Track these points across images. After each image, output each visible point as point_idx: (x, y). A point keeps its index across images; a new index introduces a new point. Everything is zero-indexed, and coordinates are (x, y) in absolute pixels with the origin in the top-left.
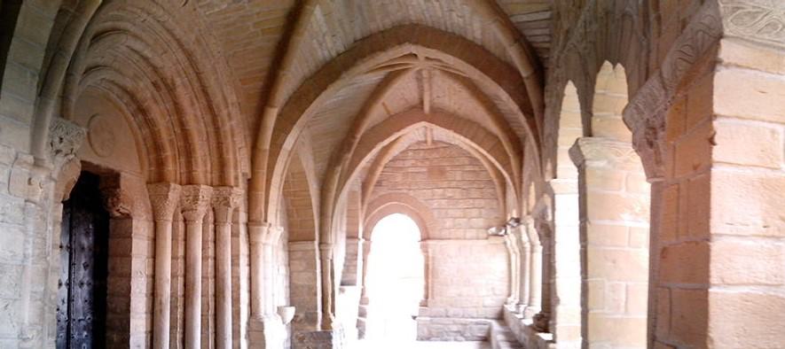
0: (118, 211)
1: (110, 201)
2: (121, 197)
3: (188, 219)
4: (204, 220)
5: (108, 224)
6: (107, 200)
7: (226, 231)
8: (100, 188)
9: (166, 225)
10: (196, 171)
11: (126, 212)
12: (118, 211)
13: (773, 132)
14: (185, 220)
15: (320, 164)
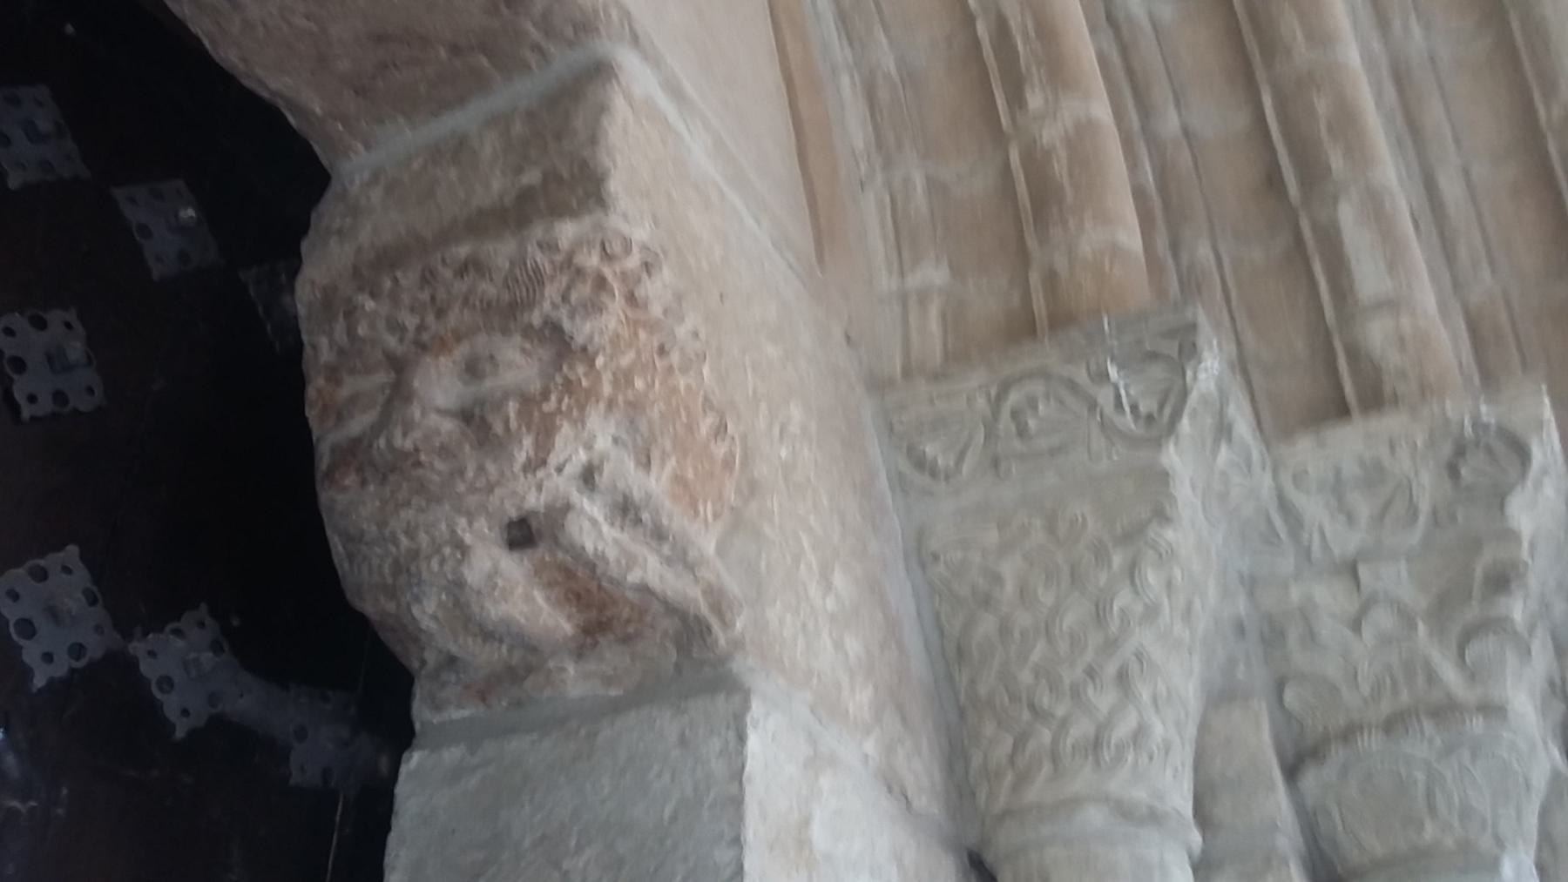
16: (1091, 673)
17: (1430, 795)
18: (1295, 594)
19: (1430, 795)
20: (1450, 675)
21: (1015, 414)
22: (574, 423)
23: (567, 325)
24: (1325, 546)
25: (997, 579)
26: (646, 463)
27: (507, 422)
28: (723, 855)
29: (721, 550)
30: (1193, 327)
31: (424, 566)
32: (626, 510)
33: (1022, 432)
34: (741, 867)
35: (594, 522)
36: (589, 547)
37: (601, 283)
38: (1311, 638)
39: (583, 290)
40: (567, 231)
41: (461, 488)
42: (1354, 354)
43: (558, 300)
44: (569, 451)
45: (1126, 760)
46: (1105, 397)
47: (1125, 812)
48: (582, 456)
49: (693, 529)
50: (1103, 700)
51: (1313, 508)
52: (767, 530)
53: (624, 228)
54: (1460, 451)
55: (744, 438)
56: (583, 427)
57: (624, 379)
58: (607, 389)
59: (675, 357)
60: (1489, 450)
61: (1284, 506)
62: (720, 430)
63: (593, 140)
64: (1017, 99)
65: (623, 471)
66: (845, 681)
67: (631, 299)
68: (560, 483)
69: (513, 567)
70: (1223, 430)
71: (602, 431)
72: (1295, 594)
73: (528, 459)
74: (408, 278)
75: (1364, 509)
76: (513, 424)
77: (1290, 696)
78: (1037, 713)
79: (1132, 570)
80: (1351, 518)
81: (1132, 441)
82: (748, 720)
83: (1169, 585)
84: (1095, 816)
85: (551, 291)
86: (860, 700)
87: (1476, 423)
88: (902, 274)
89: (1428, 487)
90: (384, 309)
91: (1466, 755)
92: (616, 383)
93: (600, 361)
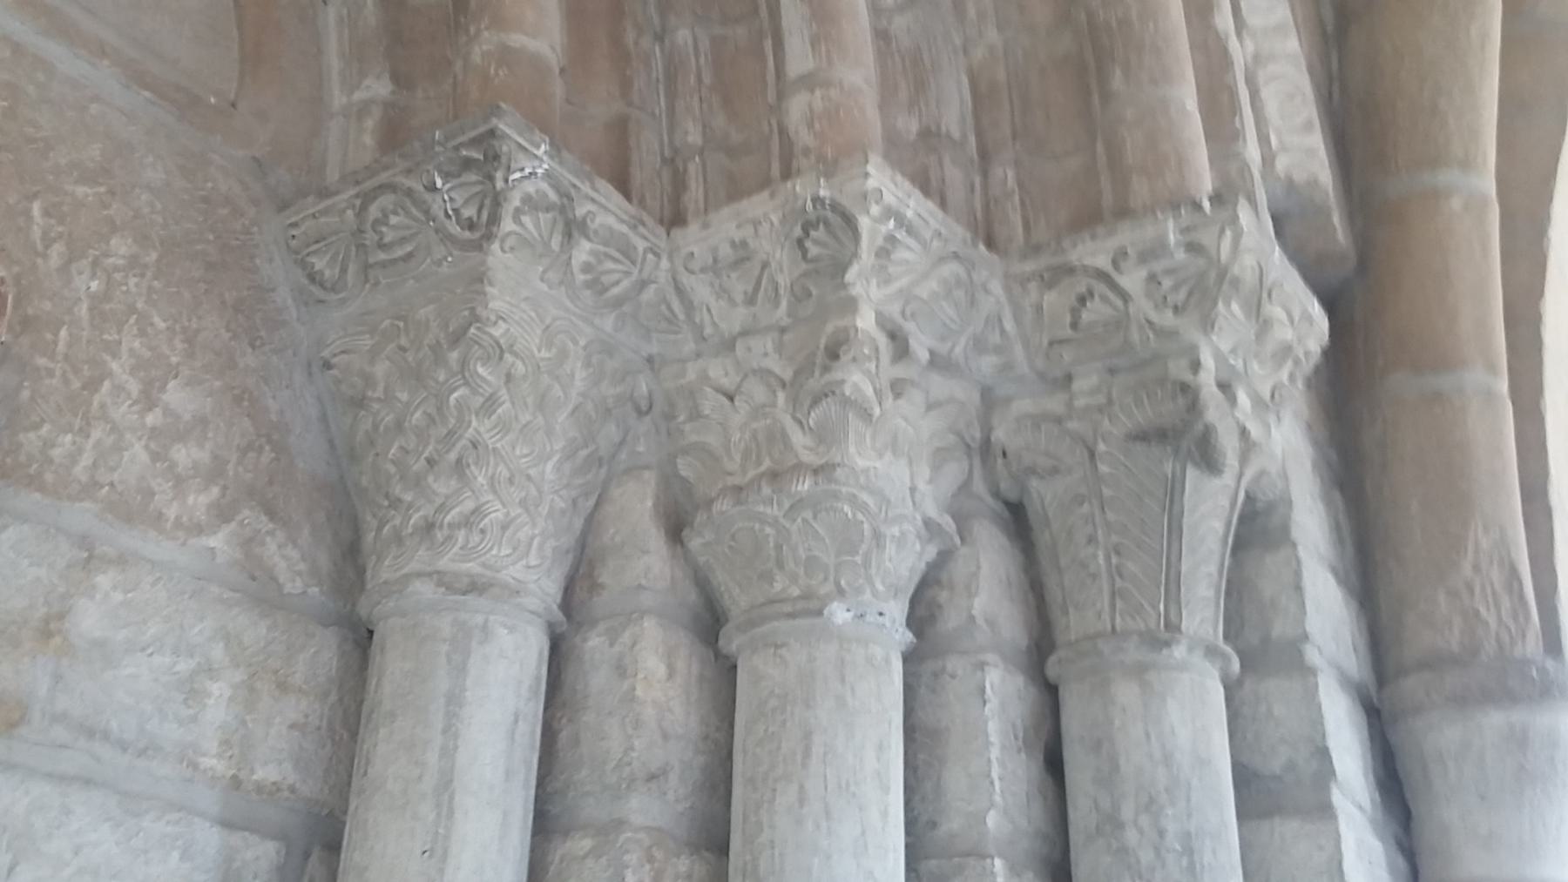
17: (779, 547)
18: (692, 373)
19: (779, 547)
20: (798, 439)
25: (369, 381)
38: (696, 415)
45: (457, 540)
46: (437, 209)
47: (445, 581)
50: (441, 486)
51: (701, 289)
54: (807, 227)
60: (827, 224)
72: (692, 373)
78: (395, 503)
81: (467, 246)
87: (817, 200)
89: (784, 266)
91: (808, 514)
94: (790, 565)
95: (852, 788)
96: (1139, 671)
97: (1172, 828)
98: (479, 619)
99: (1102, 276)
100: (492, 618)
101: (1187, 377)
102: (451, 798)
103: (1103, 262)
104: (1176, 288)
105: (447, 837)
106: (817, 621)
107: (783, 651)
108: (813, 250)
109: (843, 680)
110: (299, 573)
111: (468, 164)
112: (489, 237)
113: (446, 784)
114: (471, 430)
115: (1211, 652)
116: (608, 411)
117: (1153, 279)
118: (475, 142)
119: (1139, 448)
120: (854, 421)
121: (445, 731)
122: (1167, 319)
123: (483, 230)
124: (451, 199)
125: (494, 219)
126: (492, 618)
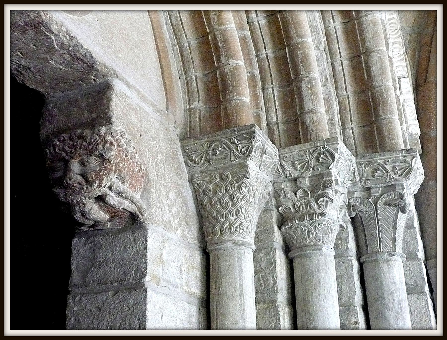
0: (101, 199)
1: (75, 167)
2: (113, 154)
3: (294, 241)
4: (336, 247)
5: (68, 253)
6: (66, 163)
7: (387, 280)
8: (43, 133)
9: (240, 257)
10: (312, 112)
11: (127, 205)
12: (101, 199)
13: (393, 44)
14: (287, 249)
15: (225, 17)
16: (230, 212)
21: (213, 150)
22: (107, 177)
23: (104, 155)
24: (290, 174)
26: (123, 183)
27: (92, 177)
28: (143, 266)
29: (142, 197)
30: (254, 132)
31: (76, 207)
32: (119, 194)
33: (215, 154)
34: (146, 268)
35: (112, 197)
36: (112, 203)
37: (111, 144)
39: (108, 145)
40: (103, 130)
41: (83, 192)
42: (303, 123)
43: (102, 148)
44: (106, 182)
47: (235, 243)
48: (109, 183)
49: (134, 194)
51: (287, 166)
52: (152, 190)
53: (117, 129)
55: (146, 170)
56: (109, 178)
57: (117, 165)
58: (114, 168)
59: (129, 156)
61: (281, 165)
62: (140, 170)
63: (108, 108)
64: (219, 59)
65: (118, 185)
66: (171, 219)
67: (118, 145)
68: (105, 190)
69: (95, 207)
70: (264, 152)
71: (113, 177)
73: (97, 186)
74: (66, 136)
75: (299, 167)
76: (94, 178)
77: (280, 209)
79: (239, 188)
80: (296, 169)
82: (148, 236)
83: (249, 191)
84: (229, 244)
85: (100, 146)
86: (175, 223)
88: (189, 104)
90: (62, 145)
92: (116, 166)
93: (112, 162)
94: (311, 237)
95: (331, 292)
96: (387, 261)
97: (396, 298)
98: (243, 252)
99: (381, 165)
100: (245, 251)
101: (401, 191)
102: (243, 296)
103: (381, 162)
104: (399, 170)
105: (244, 306)
106: (319, 251)
107: (311, 259)
108: (321, 160)
109: (326, 266)
110: (192, 238)
111: (245, 138)
112: (248, 156)
113: (242, 293)
114: (240, 204)
115: (402, 256)
116: (92, 127)
117: (394, 167)
118: (247, 133)
119: (387, 208)
120: (329, 202)
121: (240, 280)
122: (396, 177)
123: (247, 155)
124: (240, 147)
125: (250, 153)
126: (245, 251)
